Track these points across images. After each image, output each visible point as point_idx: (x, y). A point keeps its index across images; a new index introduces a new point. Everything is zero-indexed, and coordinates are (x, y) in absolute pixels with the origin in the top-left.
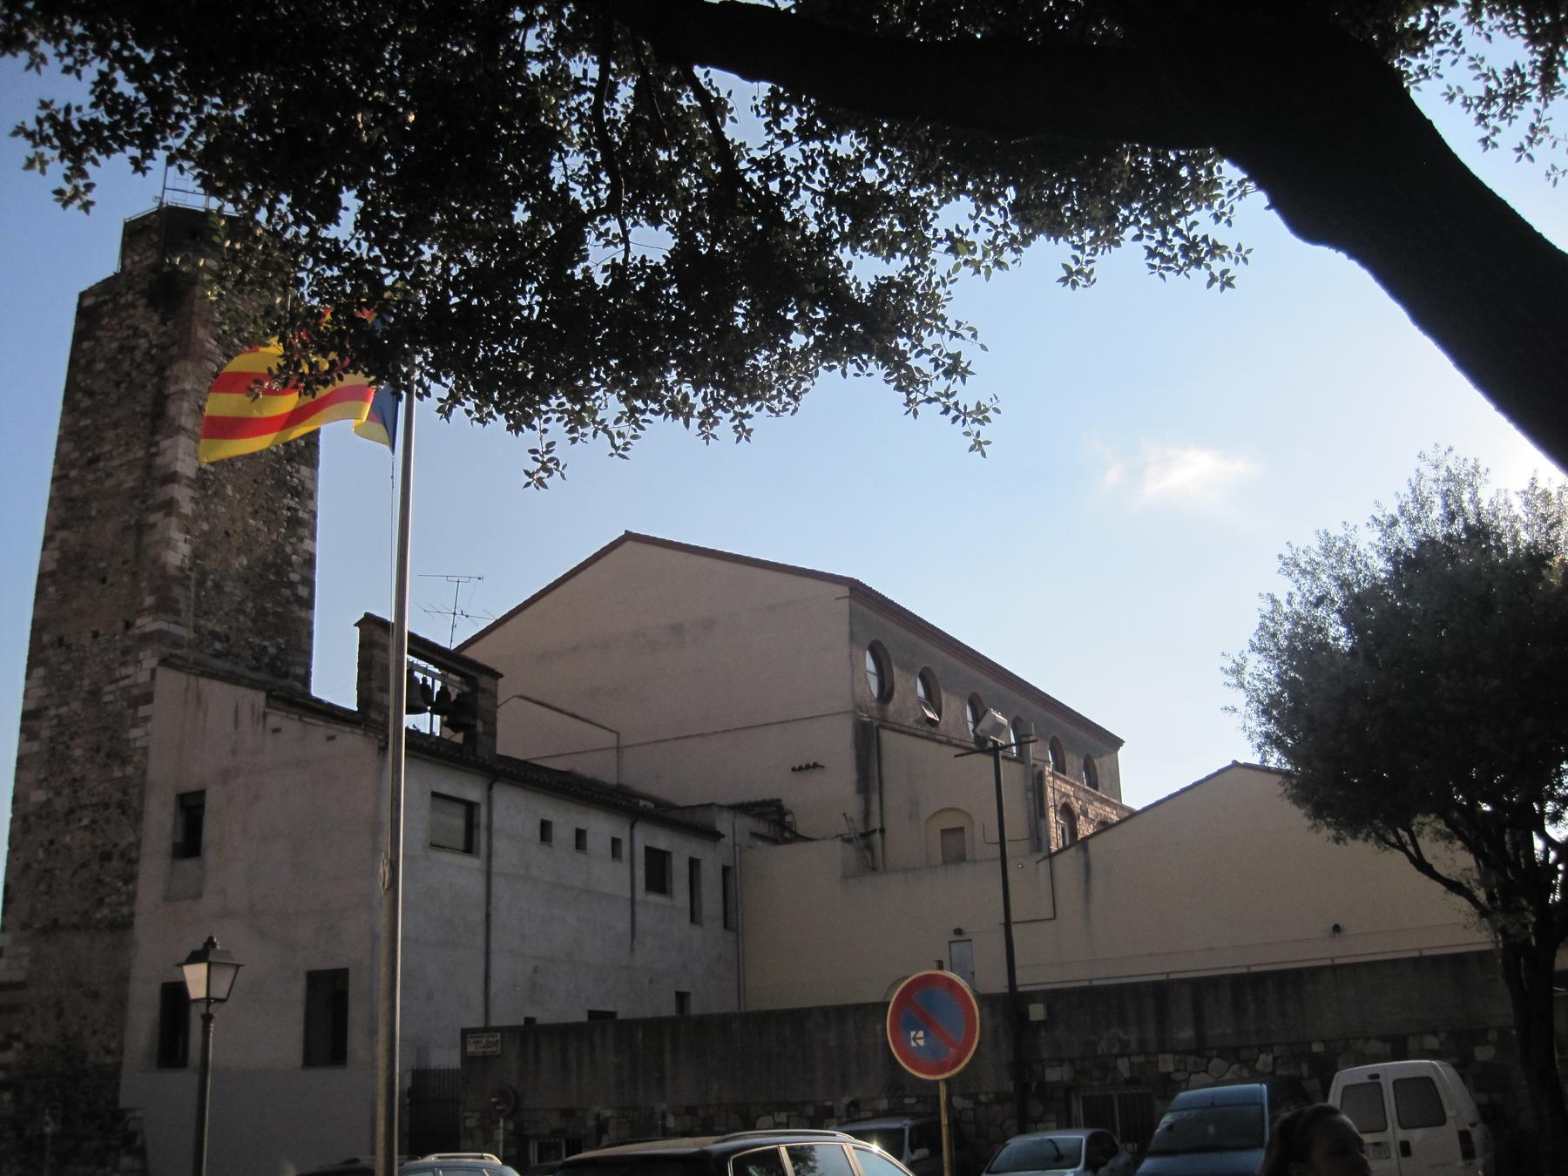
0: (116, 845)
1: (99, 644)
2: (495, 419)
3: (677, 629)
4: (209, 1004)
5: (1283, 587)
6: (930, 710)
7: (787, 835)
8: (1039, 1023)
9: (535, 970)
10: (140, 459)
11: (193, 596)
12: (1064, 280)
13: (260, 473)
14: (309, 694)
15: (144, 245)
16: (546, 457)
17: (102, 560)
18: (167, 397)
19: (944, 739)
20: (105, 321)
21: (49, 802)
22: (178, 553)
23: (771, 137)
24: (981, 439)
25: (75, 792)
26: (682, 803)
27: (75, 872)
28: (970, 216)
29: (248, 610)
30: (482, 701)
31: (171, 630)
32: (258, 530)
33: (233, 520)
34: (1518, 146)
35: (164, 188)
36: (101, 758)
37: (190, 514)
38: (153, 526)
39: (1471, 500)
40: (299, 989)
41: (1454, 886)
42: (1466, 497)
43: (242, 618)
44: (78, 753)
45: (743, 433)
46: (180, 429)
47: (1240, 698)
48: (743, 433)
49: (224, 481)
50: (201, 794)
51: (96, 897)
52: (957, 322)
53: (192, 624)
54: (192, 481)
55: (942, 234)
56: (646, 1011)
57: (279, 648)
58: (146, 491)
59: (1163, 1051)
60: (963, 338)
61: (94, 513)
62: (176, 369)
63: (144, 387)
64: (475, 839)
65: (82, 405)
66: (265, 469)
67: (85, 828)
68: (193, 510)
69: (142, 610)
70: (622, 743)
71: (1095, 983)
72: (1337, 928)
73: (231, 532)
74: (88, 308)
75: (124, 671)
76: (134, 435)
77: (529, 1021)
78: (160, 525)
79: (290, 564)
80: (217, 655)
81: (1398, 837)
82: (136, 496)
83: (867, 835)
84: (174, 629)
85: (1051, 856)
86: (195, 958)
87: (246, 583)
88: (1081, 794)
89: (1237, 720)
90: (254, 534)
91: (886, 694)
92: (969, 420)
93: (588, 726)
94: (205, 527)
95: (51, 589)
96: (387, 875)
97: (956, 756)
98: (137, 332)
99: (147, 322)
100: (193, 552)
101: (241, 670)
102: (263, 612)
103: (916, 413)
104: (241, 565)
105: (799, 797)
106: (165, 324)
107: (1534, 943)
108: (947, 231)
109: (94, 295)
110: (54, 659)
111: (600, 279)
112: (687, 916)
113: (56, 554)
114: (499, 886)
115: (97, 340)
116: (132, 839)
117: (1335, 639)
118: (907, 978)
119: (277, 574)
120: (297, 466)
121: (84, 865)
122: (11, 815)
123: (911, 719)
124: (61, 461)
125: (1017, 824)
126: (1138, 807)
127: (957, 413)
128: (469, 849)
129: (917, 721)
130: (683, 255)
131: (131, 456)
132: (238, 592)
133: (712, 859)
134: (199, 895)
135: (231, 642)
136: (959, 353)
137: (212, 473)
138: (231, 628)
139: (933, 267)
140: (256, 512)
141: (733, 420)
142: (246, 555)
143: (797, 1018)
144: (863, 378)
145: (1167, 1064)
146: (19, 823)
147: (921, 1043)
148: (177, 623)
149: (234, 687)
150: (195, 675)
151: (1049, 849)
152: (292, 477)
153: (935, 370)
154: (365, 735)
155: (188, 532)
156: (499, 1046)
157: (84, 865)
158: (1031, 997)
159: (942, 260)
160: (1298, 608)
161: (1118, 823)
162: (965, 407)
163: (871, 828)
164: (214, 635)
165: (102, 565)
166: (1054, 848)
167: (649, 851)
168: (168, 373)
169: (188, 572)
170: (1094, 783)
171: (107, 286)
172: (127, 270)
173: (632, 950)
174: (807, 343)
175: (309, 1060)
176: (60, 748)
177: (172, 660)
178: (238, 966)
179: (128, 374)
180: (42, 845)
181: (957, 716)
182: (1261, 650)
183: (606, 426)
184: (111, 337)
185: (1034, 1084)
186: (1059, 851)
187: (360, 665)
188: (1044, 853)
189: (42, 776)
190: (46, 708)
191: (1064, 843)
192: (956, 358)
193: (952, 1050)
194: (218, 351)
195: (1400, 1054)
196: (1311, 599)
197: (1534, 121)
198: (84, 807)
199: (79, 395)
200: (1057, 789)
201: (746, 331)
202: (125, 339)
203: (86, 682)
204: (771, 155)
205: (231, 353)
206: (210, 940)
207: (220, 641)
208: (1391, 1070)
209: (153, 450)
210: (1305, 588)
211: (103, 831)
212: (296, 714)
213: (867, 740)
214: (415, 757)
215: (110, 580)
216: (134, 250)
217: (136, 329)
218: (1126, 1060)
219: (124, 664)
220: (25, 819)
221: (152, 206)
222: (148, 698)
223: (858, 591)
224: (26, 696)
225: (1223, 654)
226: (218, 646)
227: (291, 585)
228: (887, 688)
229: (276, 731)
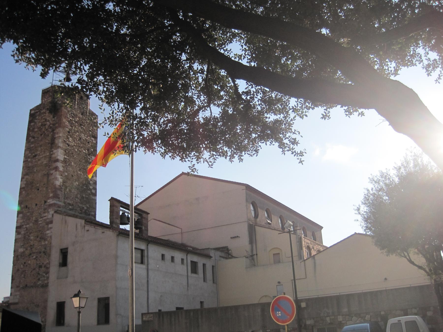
0: (43, 264)
1: (37, 207)
2: (176, 158)
3: (197, 199)
4: (80, 309)
5: (370, 186)
6: (269, 220)
7: (230, 256)
8: (304, 308)
9: (161, 296)
10: (48, 155)
11: (63, 193)
12: (322, 118)
13: (81, 159)
14: (96, 220)
15: (48, 96)
16: (193, 168)
17: (38, 184)
18: (55, 138)
19: (273, 228)
20: (37, 117)
21: (24, 252)
22: (59, 181)
23: (248, 85)
24: (302, 160)
25: (31, 249)
26: (200, 248)
27: (32, 271)
28: (296, 101)
29: (79, 197)
30: (144, 221)
31: (57, 203)
32: (81, 174)
33: (74, 172)
34: (436, 80)
35: (53, 80)
36: (38, 239)
37: (62, 170)
38: (52, 174)
39: (421, 161)
40: (96, 303)
41: (420, 267)
42: (419, 160)
43: (77, 199)
44: (32, 238)
45: (241, 160)
46: (59, 147)
47: (359, 218)
48: (241, 160)
49: (71, 161)
50: (67, 249)
51: (38, 278)
52: (295, 130)
53: (63, 201)
54: (63, 161)
55: (291, 107)
56: (192, 307)
57: (87, 208)
58: (50, 164)
59: (339, 315)
60: (296, 134)
61: (35, 171)
62: (57, 130)
63: (48, 135)
64: (144, 259)
65: (31, 141)
66: (82, 158)
67: (35, 259)
68: (63, 169)
69: (49, 198)
70: (183, 232)
71: (319, 296)
72: (386, 279)
73: (73, 175)
74: (32, 114)
75: (45, 215)
76: (46, 149)
77: (160, 310)
78: (54, 173)
79: (90, 184)
80: (70, 210)
81: (404, 254)
82: (47, 166)
83: (252, 256)
84: (58, 203)
85: (304, 260)
86: (76, 296)
87: (78, 189)
88: (312, 243)
89: (358, 223)
90: (79, 176)
91: (256, 216)
92: (298, 155)
93: (173, 227)
94: (66, 174)
95: (24, 192)
96: (130, 272)
97: (279, 234)
98: (46, 120)
99: (49, 117)
100: (63, 181)
101: (77, 214)
102: (83, 197)
103: (285, 154)
104: (76, 184)
105: (233, 245)
106: (54, 118)
107: (185, 146)
108: (292, 107)
109: (34, 110)
110: (24, 212)
111: (202, 121)
112: (212, 282)
113: (25, 182)
114: (150, 273)
115: (35, 123)
116: (48, 262)
117: (385, 200)
118: (276, 297)
119: (86, 187)
120: (91, 157)
121: (34, 269)
122: (13, 256)
123: (264, 223)
124: (26, 156)
125: (295, 253)
126: (328, 246)
127: (296, 154)
128: (142, 263)
129: (265, 224)
130: (224, 113)
131: (45, 155)
132: (76, 192)
133: (209, 264)
134: (67, 277)
135: (74, 206)
136: (296, 138)
137: (68, 159)
138: (74, 202)
139: (289, 116)
140: (80, 169)
141: (238, 157)
142: (78, 182)
143: (236, 308)
144: (272, 145)
145: (340, 318)
146: (16, 258)
147: (280, 315)
148: (59, 201)
149: (75, 219)
150: (65, 215)
151: (304, 259)
152: (90, 159)
153: (290, 143)
154: (113, 231)
155: (61, 175)
156: (152, 318)
157: (34, 269)
158: (302, 301)
159: (292, 115)
160: (374, 192)
161: (323, 251)
162: (297, 152)
163: (253, 254)
164: (69, 204)
165: (38, 185)
166: (305, 258)
167: (192, 262)
168: (55, 131)
169: (62, 187)
170: (315, 239)
171: (38, 107)
172: (43, 103)
173: (188, 290)
174: (256, 136)
175: (99, 323)
176: (27, 236)
177: (58, 211)
178: (87, 298)
179: (44, 132)
180: (22, 264)
181: (276, 222)
182: (365, 204)
183: (207, 160)
184: (39, 122)
185: (303, 325)
186: (306, 259)
187: (110, 212)
188: (303, 260)
189: (22, 244)
190: (23, 225)
191: (308, 257)
192: (295, 139)
193: (288, 317)
194: (69, 125)
195: (406, 314)
196: (378, 189)
197: (440, 74)
198: (34, 253)
199: (30, 138)
200: (305, 242)
201: (240, 133)
202: (43, 122)
203: (34, 218)
204: (248, 90)
205: (72, 125)
206: (80, 291)
207: (71, 206)
208: (404, 319)
209: (52, 153)
210: (376, 186)
211: (40, 260)
212: (93, 226)
213: (252, 229)
214: (137, 240)
215: (40, 190)
216: (45, 98)
217: (46, 120)
218: (329, 318)
219: (44, 213)
220: (17, 256)
221: (50, 85)
222: (51, 222)
223: (248, 187)
224: (17, 222)
225: (354, 205)
226: (70, 207)
227: (90, 190)
228: (257, 215)
229: (88, 231)
